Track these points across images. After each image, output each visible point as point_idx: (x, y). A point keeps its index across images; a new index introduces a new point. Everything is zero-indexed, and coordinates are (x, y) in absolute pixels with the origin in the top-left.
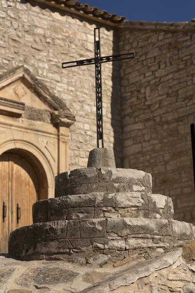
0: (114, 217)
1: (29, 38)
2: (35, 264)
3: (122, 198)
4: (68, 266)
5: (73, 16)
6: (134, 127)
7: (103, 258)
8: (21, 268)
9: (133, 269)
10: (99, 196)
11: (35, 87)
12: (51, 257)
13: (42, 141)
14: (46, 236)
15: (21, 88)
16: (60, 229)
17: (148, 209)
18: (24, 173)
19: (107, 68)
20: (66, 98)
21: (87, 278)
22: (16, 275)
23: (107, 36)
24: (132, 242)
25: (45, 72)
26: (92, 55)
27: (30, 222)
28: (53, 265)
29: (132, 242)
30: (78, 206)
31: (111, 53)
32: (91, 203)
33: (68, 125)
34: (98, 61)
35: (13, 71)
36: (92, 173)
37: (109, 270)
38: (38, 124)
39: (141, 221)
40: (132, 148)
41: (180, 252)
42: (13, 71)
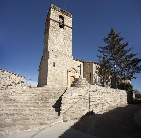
0: (82, 83)
1: (74, 64)
2: (73, 88)
3: (83, 81)
4: (76, 88)
5: (79, 61)
6: (85, 73)
7: (80, 87)
8: (72, 88)
9: (83, 88)
10: (80, 81)
11: (75, 69)
12: (75, 87)
13: (75, 75)
14: (75, 85)
15: (73, 69)
16: (20, 131)
17: (85, 82)
18: (73, 78)
19: (82, 67)
20: (78, 70)
21: (79, 89)
22: (71, 89)
23: (82, 64)
24: (83, 86)
25: (76, 68)
26: (80, 67)
27: (73, 83)
28: (75, 88)
29: (83, 86)
30: (78, 82)
31: (83, 65)
32: (79, 82)
33: (78, 73)
34: (81, 66)
35: (72, 67)
36: (80, 78)
37: (81, 88)
38: (75, 73)
39: (85, 83)
40: (85, 76)
41: (89, 87)
42: (72, 67)
